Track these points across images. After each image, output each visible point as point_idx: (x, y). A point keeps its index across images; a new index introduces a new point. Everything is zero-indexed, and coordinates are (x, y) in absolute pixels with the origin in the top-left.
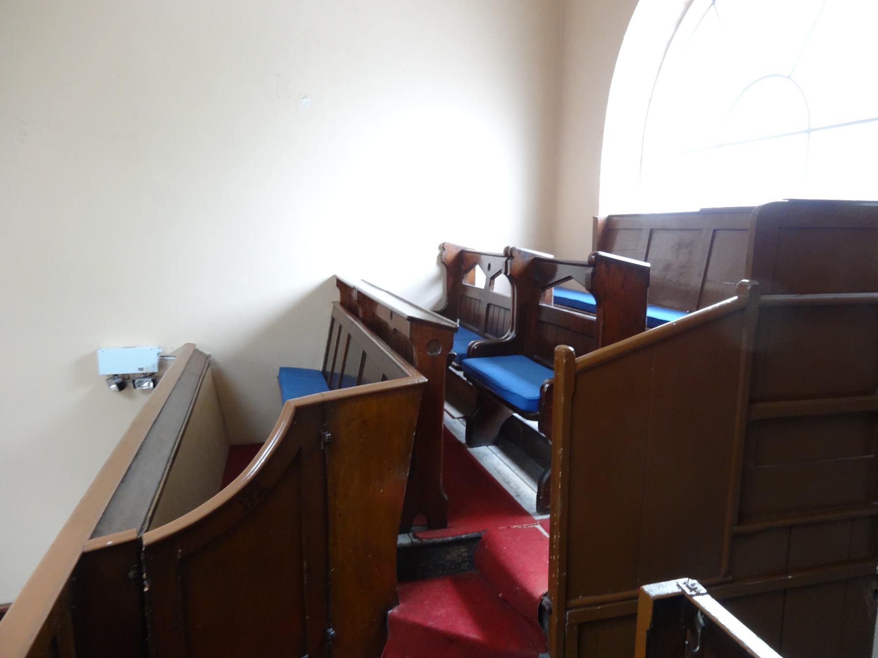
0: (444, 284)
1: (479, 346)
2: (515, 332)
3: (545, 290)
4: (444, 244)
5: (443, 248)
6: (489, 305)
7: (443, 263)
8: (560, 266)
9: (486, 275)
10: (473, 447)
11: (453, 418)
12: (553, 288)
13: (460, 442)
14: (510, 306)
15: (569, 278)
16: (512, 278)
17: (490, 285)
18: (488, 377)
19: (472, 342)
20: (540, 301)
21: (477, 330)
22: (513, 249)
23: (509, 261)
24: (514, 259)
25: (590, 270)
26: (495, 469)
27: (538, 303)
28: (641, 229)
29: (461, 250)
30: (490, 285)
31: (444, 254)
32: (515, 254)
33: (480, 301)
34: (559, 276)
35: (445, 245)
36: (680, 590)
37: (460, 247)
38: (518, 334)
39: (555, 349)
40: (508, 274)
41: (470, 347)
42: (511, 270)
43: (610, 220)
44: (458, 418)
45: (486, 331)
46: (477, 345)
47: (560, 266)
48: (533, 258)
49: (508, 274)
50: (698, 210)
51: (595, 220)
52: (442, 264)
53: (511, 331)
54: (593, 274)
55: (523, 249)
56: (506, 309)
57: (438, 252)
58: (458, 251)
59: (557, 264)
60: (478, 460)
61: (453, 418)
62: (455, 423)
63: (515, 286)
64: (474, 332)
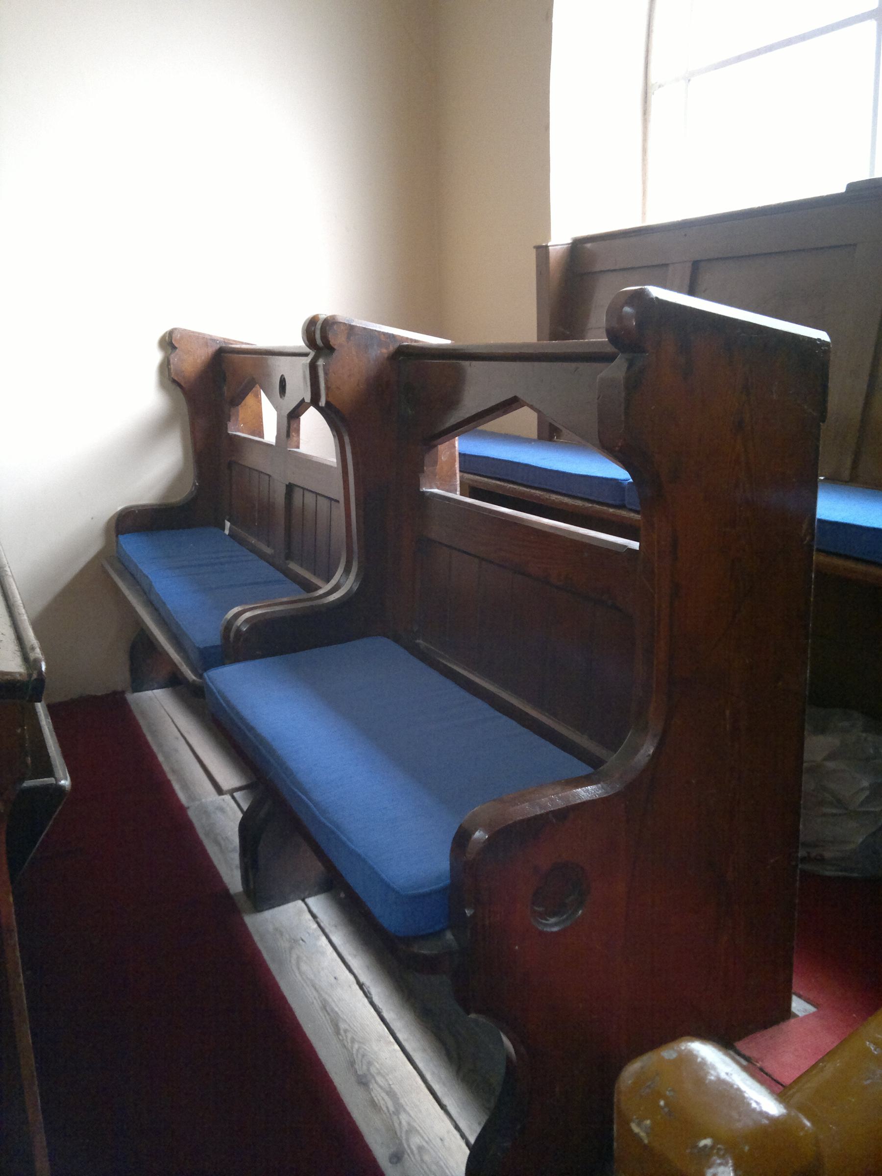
0: (184, 438)
1: (256, 624)
2: (357, 575)
3: (436, 446)
4: (171, 333)
5: (169, 343)
6: (290, 488)
7: (174, 381)
8: (473, 369)
9: (276, 408)
10: (261, 911)
11: (220, 791)
12: (457, 438)
13: (226, 890)
14: (337, 492)
15: (510, 404)
16: (330, 413)
17: (288, 435)
18: (272, 751)
19: (236, 610)
20: (422, 480)
21: (269, 551)
22: (329, 324)
23: (321, 362)
24: (335, 354)
25: (617, 370)
26: (325, 1006)
27: (418, 486)
28: (667, 265)
29: (218, 346)
30: (288, 435)
31: (174, 359)
32: (337, 340)
33: (270, 476)
34: (471, 403)
35: (177, 336)
36: (739, 1045)
37: (214, 340)
38: (364, 578)
39: (634, 1067)
40: (322, 403)
41: (230, 624)
42: (328, 388)
43: (578, 246)
44: (231, 792)
45: (289, 556)
46: (247, 621)
47: (473, 369)
48: (392, 348)
49: (322, 403)
50: (842, 189)
51: (542, 251)
52: (173, 386)
53: (347, 571)
54: (633, 384)
55: (360, 323)
56: (331, 499)
57: (157, 356)
58: (211, 350)
59: (466, 364)
60: (273, 967)
61: (220, 791)
62: (222, 810)
63: (347, 439)
64: (262, 556)
